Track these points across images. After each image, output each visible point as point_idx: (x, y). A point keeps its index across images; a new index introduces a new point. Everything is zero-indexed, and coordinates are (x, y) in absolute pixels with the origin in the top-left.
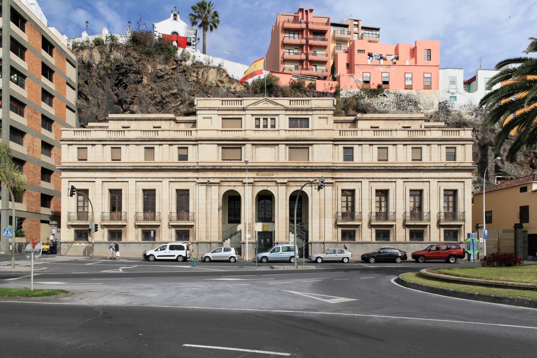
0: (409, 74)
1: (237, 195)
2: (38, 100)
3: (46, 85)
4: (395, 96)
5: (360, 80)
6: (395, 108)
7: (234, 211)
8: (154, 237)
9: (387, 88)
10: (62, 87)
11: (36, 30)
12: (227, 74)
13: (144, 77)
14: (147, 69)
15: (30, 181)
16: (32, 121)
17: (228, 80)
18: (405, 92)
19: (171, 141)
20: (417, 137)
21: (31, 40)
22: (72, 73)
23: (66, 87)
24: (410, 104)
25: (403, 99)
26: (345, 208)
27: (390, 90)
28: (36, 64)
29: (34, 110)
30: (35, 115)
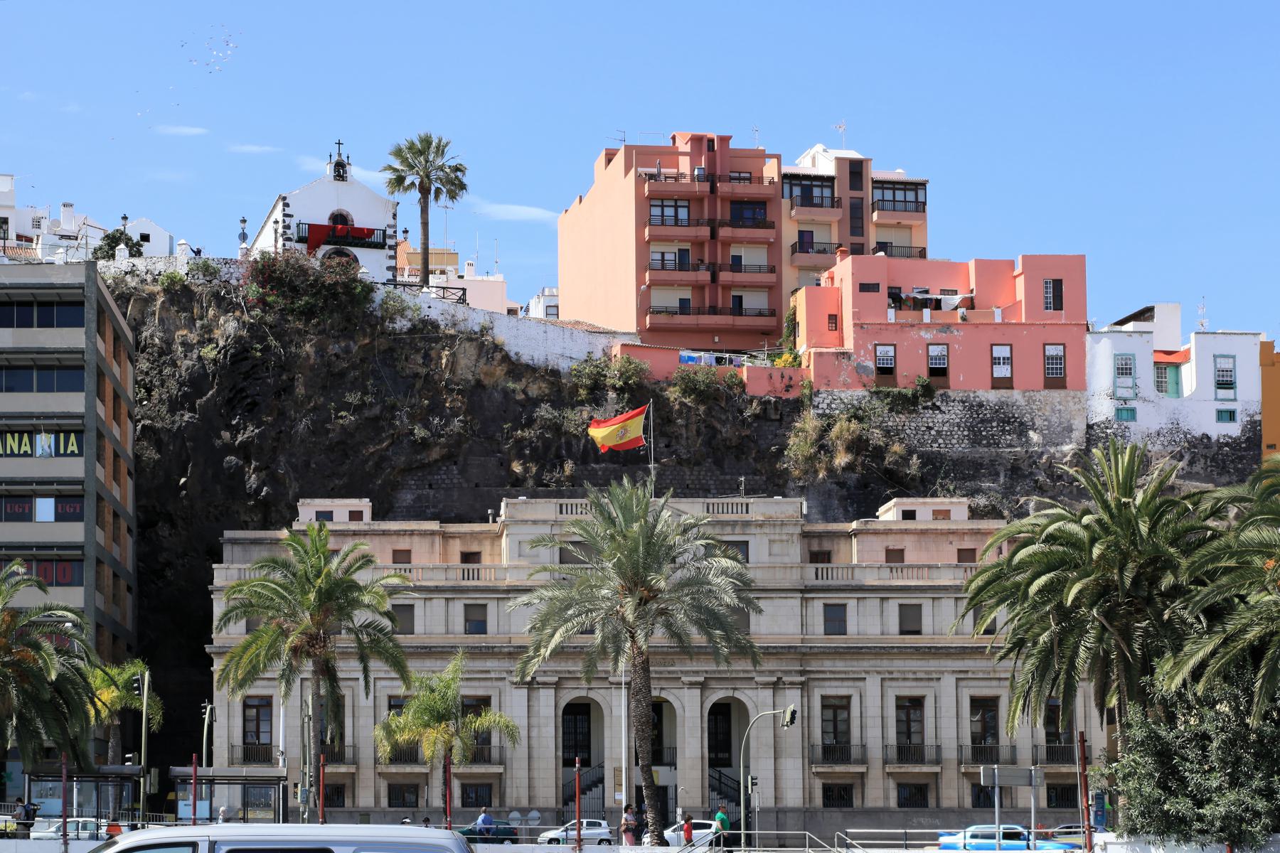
4: (965, 407)
6: (966, 441)
17: (505, 369)
18: (992, 397)
27: (950, 393)
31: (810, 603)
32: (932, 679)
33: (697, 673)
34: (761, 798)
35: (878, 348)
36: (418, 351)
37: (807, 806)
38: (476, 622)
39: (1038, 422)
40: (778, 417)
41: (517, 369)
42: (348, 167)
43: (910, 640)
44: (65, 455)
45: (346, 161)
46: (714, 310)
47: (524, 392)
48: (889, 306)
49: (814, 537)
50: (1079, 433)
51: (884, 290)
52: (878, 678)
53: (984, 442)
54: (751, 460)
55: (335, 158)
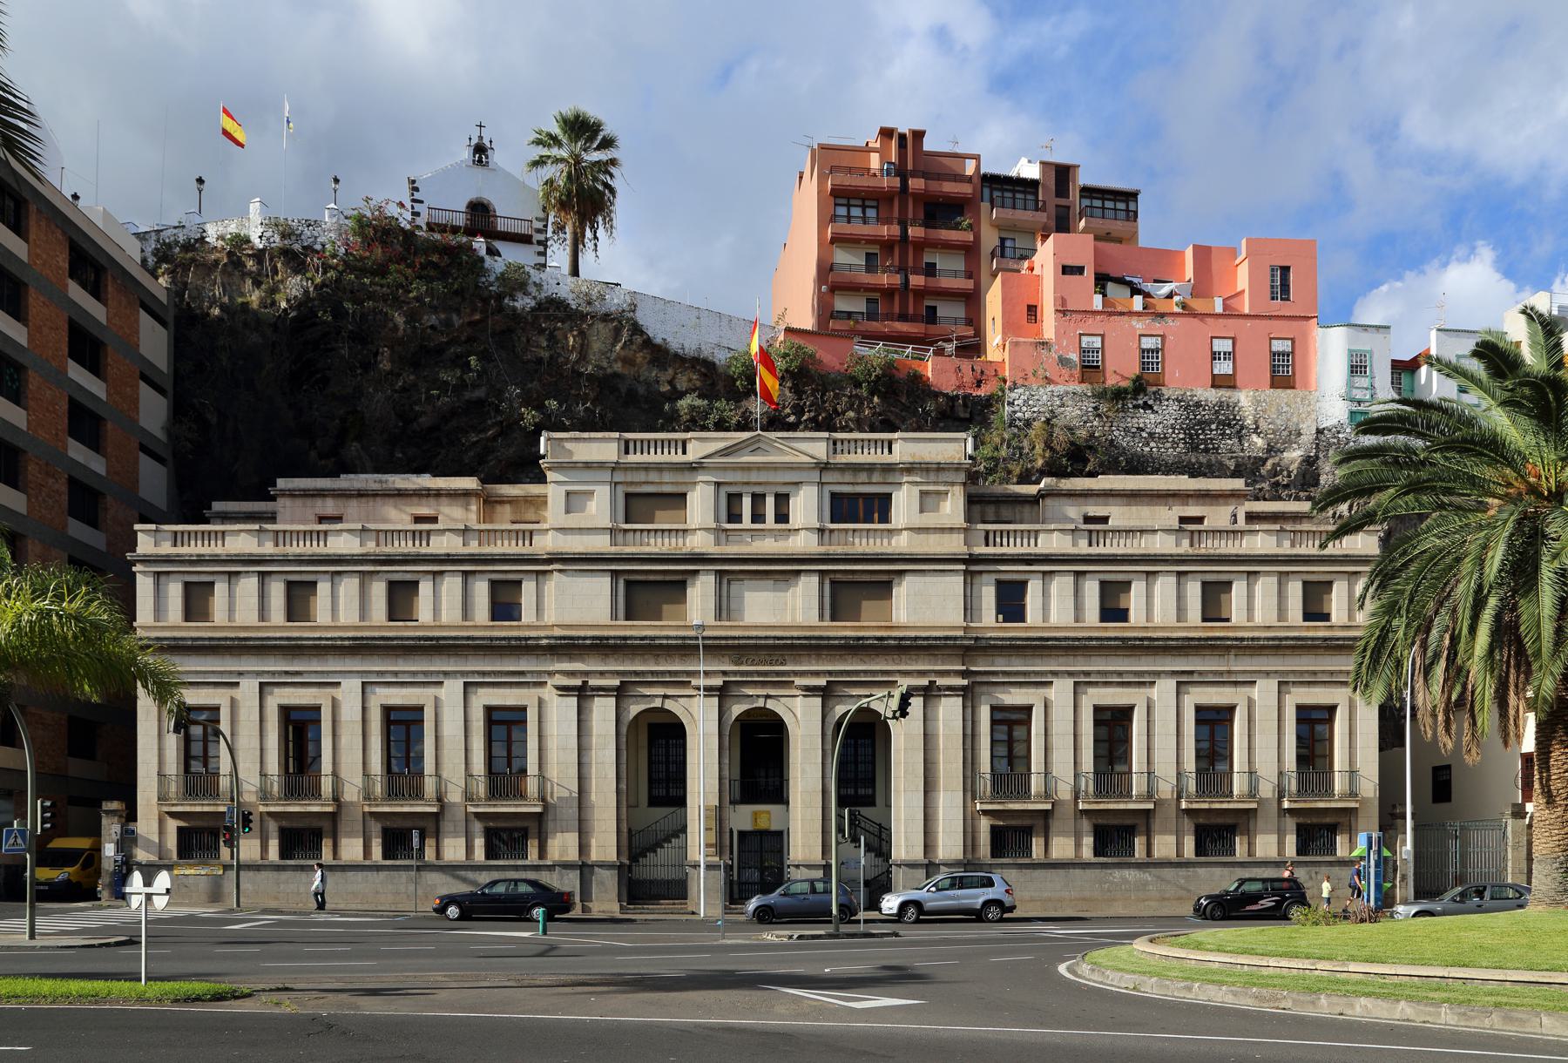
0: (1226, 341)
1: (675, 721)
2: (57, 434)
4: (1181, 407)
6: (1181, 445)
8: (420, 849)
9: (1157, 385)
10: (128, 389)
12: (645, 337)
13: (381, 350)
14: (391, 325)
16: (40, 498)
18: (1211, 396)
19: (468, 565)
20: (1218, 552)
21: (38, 256)
22: (154, 342)
23: (138, 387)
24: (1228, 432)
25: (1207, 417)
26: (1005, 761)
27: (1164, 390)
28: (52, 328)
29: (47, 464)
30: (51, 481)
31: (977, 580)
32: (1144, 681)
33: (817, 674)
34: (905, 843)
35: (1083, 338)
36: (541, 331)
37: (969, 856)
38: (504, 605)
39: (1263, 425)
41: (660, 354)
42: (490, 152)
43: (1114, 629)
45: (488, 145)
46: (903, 317)
47: (670, 382)
48: (1095, 292)
49: (989, 502)
50: (1308, 436)
51: (1089, 274)
52: (1070, 682)
53: (1202, 447)
55: (475, 141)
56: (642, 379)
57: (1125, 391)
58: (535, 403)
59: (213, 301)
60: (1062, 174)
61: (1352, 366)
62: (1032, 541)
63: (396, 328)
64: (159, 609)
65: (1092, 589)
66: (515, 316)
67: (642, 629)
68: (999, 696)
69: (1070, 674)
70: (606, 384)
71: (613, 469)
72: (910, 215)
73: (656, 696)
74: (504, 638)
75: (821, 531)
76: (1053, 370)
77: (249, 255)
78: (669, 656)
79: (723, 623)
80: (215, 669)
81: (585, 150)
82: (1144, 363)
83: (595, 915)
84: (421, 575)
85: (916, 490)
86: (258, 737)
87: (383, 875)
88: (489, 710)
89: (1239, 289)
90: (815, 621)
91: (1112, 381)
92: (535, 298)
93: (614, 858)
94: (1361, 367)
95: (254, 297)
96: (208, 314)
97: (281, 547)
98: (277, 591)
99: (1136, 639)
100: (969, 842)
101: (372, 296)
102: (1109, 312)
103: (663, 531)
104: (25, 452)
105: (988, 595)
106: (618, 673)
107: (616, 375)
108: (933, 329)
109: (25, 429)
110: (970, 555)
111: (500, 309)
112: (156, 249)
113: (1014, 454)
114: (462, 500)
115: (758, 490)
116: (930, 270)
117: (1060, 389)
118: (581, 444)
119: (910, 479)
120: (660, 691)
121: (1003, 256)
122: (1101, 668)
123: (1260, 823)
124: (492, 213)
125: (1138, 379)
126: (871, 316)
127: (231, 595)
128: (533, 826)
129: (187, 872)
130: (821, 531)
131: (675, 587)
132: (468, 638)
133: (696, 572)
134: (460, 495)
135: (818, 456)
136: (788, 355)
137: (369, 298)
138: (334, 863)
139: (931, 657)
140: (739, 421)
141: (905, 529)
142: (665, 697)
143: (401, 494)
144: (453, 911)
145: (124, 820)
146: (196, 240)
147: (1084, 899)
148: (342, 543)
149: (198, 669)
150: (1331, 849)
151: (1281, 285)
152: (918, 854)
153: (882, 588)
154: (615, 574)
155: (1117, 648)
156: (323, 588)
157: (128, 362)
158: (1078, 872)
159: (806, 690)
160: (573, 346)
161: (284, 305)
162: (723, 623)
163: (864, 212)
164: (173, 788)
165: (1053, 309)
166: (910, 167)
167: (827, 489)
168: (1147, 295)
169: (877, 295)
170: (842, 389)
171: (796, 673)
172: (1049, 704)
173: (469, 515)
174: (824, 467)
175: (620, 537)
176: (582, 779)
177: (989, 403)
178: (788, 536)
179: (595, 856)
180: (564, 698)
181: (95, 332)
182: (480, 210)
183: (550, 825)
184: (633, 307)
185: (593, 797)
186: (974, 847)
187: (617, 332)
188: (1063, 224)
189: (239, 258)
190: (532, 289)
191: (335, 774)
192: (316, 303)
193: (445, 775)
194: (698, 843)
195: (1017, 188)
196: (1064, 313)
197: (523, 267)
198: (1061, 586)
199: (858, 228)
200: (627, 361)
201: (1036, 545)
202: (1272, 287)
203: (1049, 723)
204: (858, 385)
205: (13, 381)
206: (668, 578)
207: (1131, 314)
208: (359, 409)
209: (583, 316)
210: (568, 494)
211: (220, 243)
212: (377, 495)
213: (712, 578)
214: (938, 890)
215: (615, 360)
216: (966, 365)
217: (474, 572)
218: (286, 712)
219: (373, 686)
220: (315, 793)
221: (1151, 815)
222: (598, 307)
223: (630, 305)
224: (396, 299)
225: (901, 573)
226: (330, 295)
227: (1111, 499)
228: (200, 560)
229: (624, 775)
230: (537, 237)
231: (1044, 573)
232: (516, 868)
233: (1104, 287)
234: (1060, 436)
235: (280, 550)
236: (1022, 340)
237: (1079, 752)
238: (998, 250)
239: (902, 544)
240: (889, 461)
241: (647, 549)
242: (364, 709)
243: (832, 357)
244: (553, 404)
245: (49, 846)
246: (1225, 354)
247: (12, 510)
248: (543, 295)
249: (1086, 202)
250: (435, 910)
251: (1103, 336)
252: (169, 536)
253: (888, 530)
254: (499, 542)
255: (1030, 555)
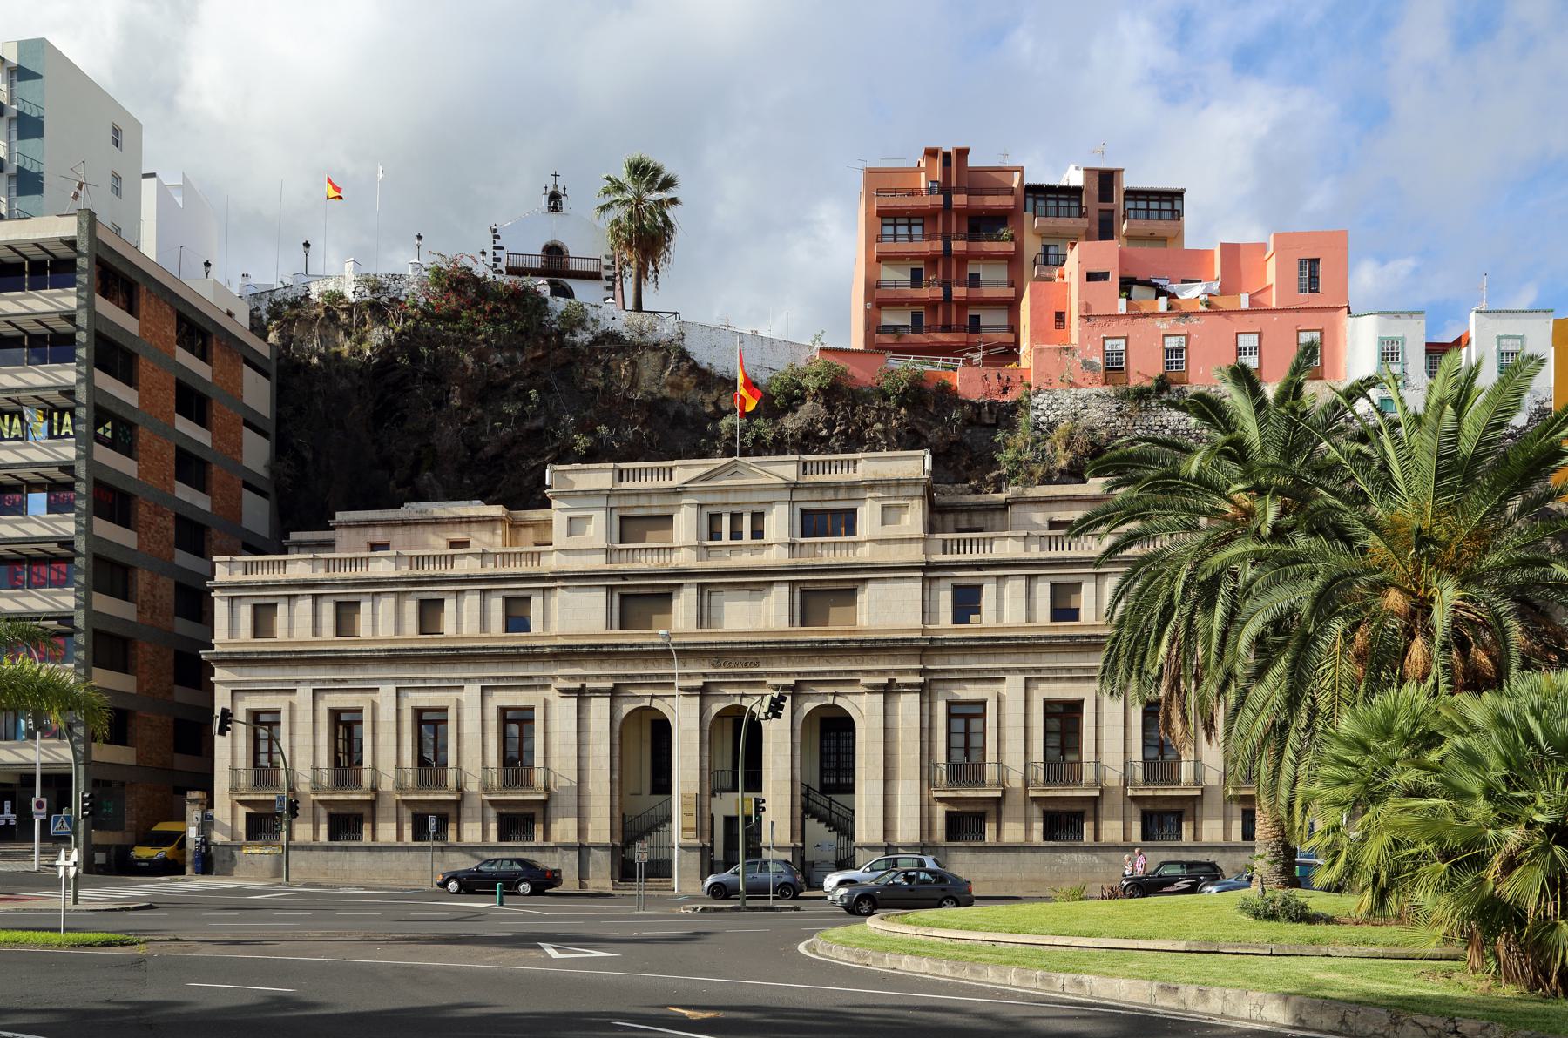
3: (187, 437)
5: (1093, 363)
7: (838, 759)
10: (232, 435)
11: (162, 302)
12: (691, 363)
14: (461, 365)
15: (146, 688)
16: (149, 535)
17: (695, 381)
19: (484, 584)
21: (148, 329)
22: (257, 392)
23: (241, 432)
26: (962, 752)
27: (1188, 387)
28: (160, 389)
29: (156, 505)
30: (159, 519)
31: (935, 585)
33: (787, 674)
34: (867, 828)
36: (597, 363)
38: (516, 620)
40: (994, 421)
41: (707, 379)
42: (563, 199)
43: (1065, 628)
44: (59, 437)
45: (562, 192)
46: (946, 328)
48: (1120, 296)
49: (962, 511)
51: (1114, 280)
52: (1021, 678)
54: (961, 468)
55: (550, 189)
56: (689, 401)
57: (1149, 391)
58: (589, 429)
59: (313, 352)
60: (1107, 179)
61: (1383, 354)
62: (987, 548)
63: (465, 368)
64: (232, 629)
65: (1043, 591)
66: (575, 349)
67: (634, 637)
68: (954, 692)
69: (1022, 670)
70: (655, 408)
71: (609, 496)
72: (954, 230)
73: (645, 696)
74: (514, 648)
75: (792, 545)
76: (1077, 374)
77: (343, 309)
78: (656, 660)
79: (703, 630)
80: (277, 678)
81: (649, 191)
82: (1167, 362)
83: (590, 890)
84: (445, 594)
85: (878, 505)
86: (311, 736)
87: (413, 854)
88: (503, 711)
89: (1268, 284)
90: (785, 626)
91: (1135, 381)
92: (592, 333)
93: (607, 840)
94: (1392, 354)
95: (345, 346)
96: (309, 363)
97: (331, 572)
98: (328, 610)
99: (1083, 637)
100: (926, 827)
101: (446, 341)
102: (1134, 314)
103: (652, 549)
104: (136, 496)
105: (945, 600)
106: (612, 676)
107: (665, 399)
108: (975, 338)
109: (136, 477)
110: (927, 562)
111: (561, 344)
112: (269, 307)
113: (1037, 457)
114: (489, 526)
115: (736, 510)
116: (974, 281)
117: (1084, 392)
118: (581, 475)
119: (873, 495)
120: (649, 692)
121: (1046, 263)
122: (1051, 665)
123: (1206, 809)
124: (565, 254)
125: (1162, 377)
126: (917, 325)
127: (290, 615)
128: (538, 812)
129: (253, 851)
130: (792, 545)
131: (663, 599)
132: (484, 648)
133: (681, 585)
134: (488, 521)
135: (789, 477)
136: (820, 374)
137: (443, 343)
138: (372, 844)
139: (892, 658)
140: (774, 438)
141: (868, 541)
142: (653, 697)
143: (437, 522)
144: (453, 886)
145: (205, 807)
146: (302, 298)
147: (1033, 880)
148: (382, 568)
149: (263, 678)
150: (981, 833)
151: (1310, 277)
152: (878, 838)
153: (847, 594)
154: (610, 589)
155: (1066, 645)
156: (365, 607)
157: (232, 411)
158: (1028, 855)
159: (868, 688)
160: (625, 375)
161: (368, 353)
162: (703, 630)
163: (910, 230)
164: (243, 780)
165: (1077, 316)
166: (954, 184)
167: (798, 507)
168: (1172, 296)
169: (921, 308)
170: (872, 402)
171: (768, 674)
172: (1001, 698)
173: (494, 540)
174: (794, 487)
175: (615, 556)
176: (580, 770)
177: (1014, 408)
178: (763, 550)
179: (591, 838)
180: (566, 700)
181: (201, 389)
182: (554, 251)
183: (553, 812)
184: (682, 336)
185: (590, 786)
186: (931, 831)
187: (666, 360)
188: (1106, 230)
189: (335, 312)
190: (590, 324)
191: (374, 768)
192: (396, 349)
193: (465, 767)
194: (680, 830)
195: (1060, 196)
196: (1088, 318)
197: (582, 305)
198: (1014, 589)
199: (904, 246)
200: (676, 386)
201: (991, 551)
202: (1301, 280)
203: (1002, 717)
204: (886, 398)
205: (126, 438)
206: (656, 591)
207: (1155, 315)
208: (432, 441)
209: (635, 347)
210: (570, 519)
211: (320, 300)
212: (417, 524)
213: (694, 590)
214: (872, 870)
215: (664, 386)
216: (992, 373)
217: (490, 590)
218: (335, 714)
219: (406, 691)
220: (358, 783)
221: (1100, 802)
222: (650, 338)
223: (678, 334)
224: (466, 341)
225: (865, 581)
226: (408, 343)
227: (1075, 504)
228: (265, 586)
229: (617, 766)
230: (605, 273)
231: (998, 577)
232: (524, 849)
233: (1129, 291)
234: (1082, 440)
235: (331, 575)
236: (1047, 346)
237: (1030, 743)
238: (1040, 259)
239: (865, 555)
240: (854, 479)
241: (637, 566)
242: (398, 711)
243: (863, 374)
244: (603, 429)
245: (154, 829)
246: (1251, 348)
247: (123, 546)
248: (600, 329)
249: (1131, 205)
250: (439, 885)
251: (1126, 339)
252: (242, 566)
253: (853, 542)
254: (512, 563)
255: (984, 561)
